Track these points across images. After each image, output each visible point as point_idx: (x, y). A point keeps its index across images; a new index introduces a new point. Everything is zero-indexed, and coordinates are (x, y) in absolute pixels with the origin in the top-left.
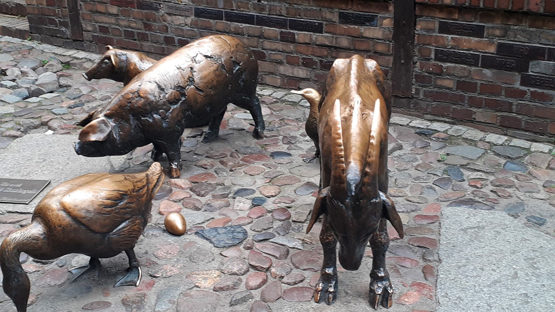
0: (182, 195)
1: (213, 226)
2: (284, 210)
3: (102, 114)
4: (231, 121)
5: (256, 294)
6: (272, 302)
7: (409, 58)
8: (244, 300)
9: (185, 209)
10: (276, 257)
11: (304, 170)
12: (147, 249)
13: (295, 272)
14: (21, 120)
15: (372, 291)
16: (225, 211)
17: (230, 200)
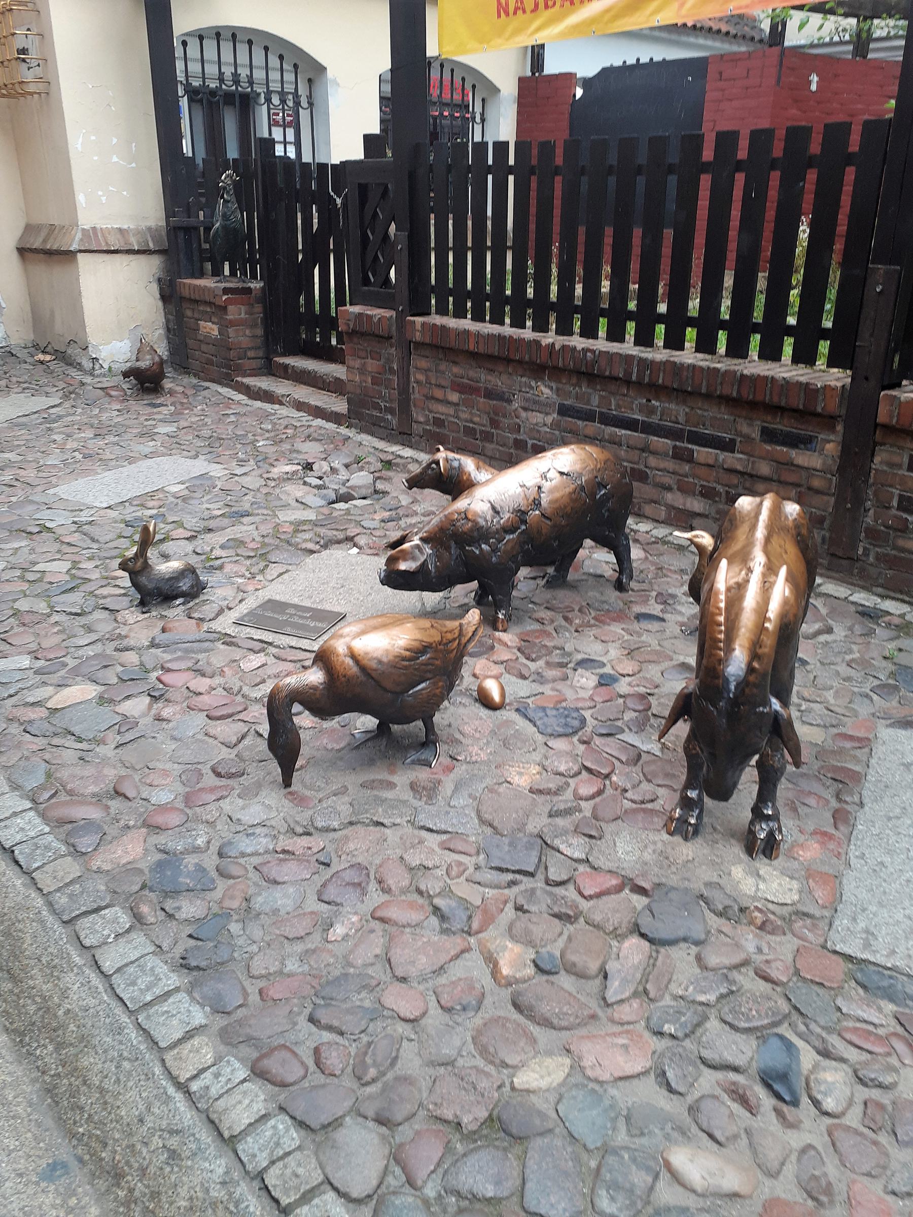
0: (505, 655)
1: (540, 703)
2: (643, 697)
3: (417, 537)
4: (587, 563)
5: (587, 806)
6: (607, 822)
7: (859, 501)
8: (568, 812)
9: (507, 675)
10: (621, 762)
11: (680, 644)
12: (452, 720)
13: (645, 786)
14: (322, 531)
15: (751, 833)
16: (560, 686)
17: (569, 672)
